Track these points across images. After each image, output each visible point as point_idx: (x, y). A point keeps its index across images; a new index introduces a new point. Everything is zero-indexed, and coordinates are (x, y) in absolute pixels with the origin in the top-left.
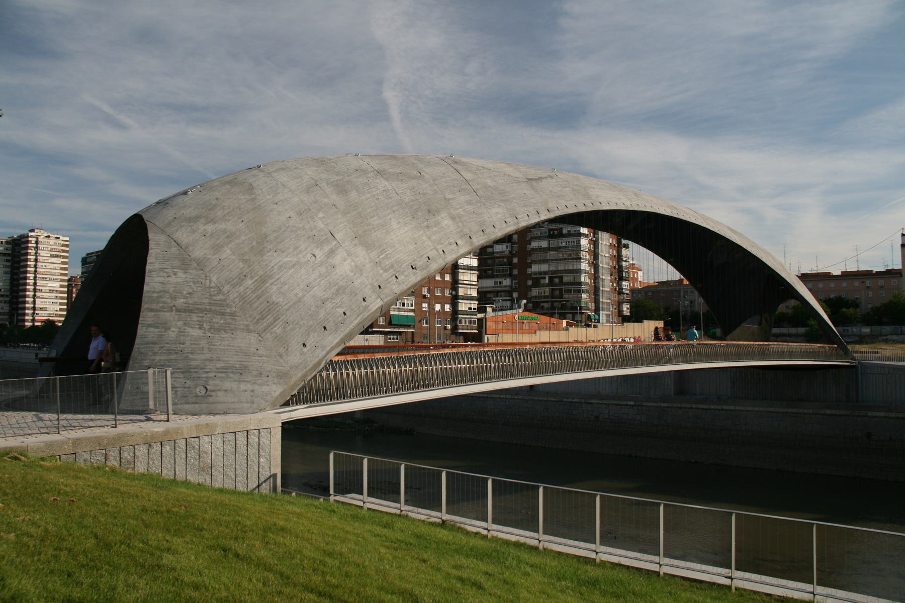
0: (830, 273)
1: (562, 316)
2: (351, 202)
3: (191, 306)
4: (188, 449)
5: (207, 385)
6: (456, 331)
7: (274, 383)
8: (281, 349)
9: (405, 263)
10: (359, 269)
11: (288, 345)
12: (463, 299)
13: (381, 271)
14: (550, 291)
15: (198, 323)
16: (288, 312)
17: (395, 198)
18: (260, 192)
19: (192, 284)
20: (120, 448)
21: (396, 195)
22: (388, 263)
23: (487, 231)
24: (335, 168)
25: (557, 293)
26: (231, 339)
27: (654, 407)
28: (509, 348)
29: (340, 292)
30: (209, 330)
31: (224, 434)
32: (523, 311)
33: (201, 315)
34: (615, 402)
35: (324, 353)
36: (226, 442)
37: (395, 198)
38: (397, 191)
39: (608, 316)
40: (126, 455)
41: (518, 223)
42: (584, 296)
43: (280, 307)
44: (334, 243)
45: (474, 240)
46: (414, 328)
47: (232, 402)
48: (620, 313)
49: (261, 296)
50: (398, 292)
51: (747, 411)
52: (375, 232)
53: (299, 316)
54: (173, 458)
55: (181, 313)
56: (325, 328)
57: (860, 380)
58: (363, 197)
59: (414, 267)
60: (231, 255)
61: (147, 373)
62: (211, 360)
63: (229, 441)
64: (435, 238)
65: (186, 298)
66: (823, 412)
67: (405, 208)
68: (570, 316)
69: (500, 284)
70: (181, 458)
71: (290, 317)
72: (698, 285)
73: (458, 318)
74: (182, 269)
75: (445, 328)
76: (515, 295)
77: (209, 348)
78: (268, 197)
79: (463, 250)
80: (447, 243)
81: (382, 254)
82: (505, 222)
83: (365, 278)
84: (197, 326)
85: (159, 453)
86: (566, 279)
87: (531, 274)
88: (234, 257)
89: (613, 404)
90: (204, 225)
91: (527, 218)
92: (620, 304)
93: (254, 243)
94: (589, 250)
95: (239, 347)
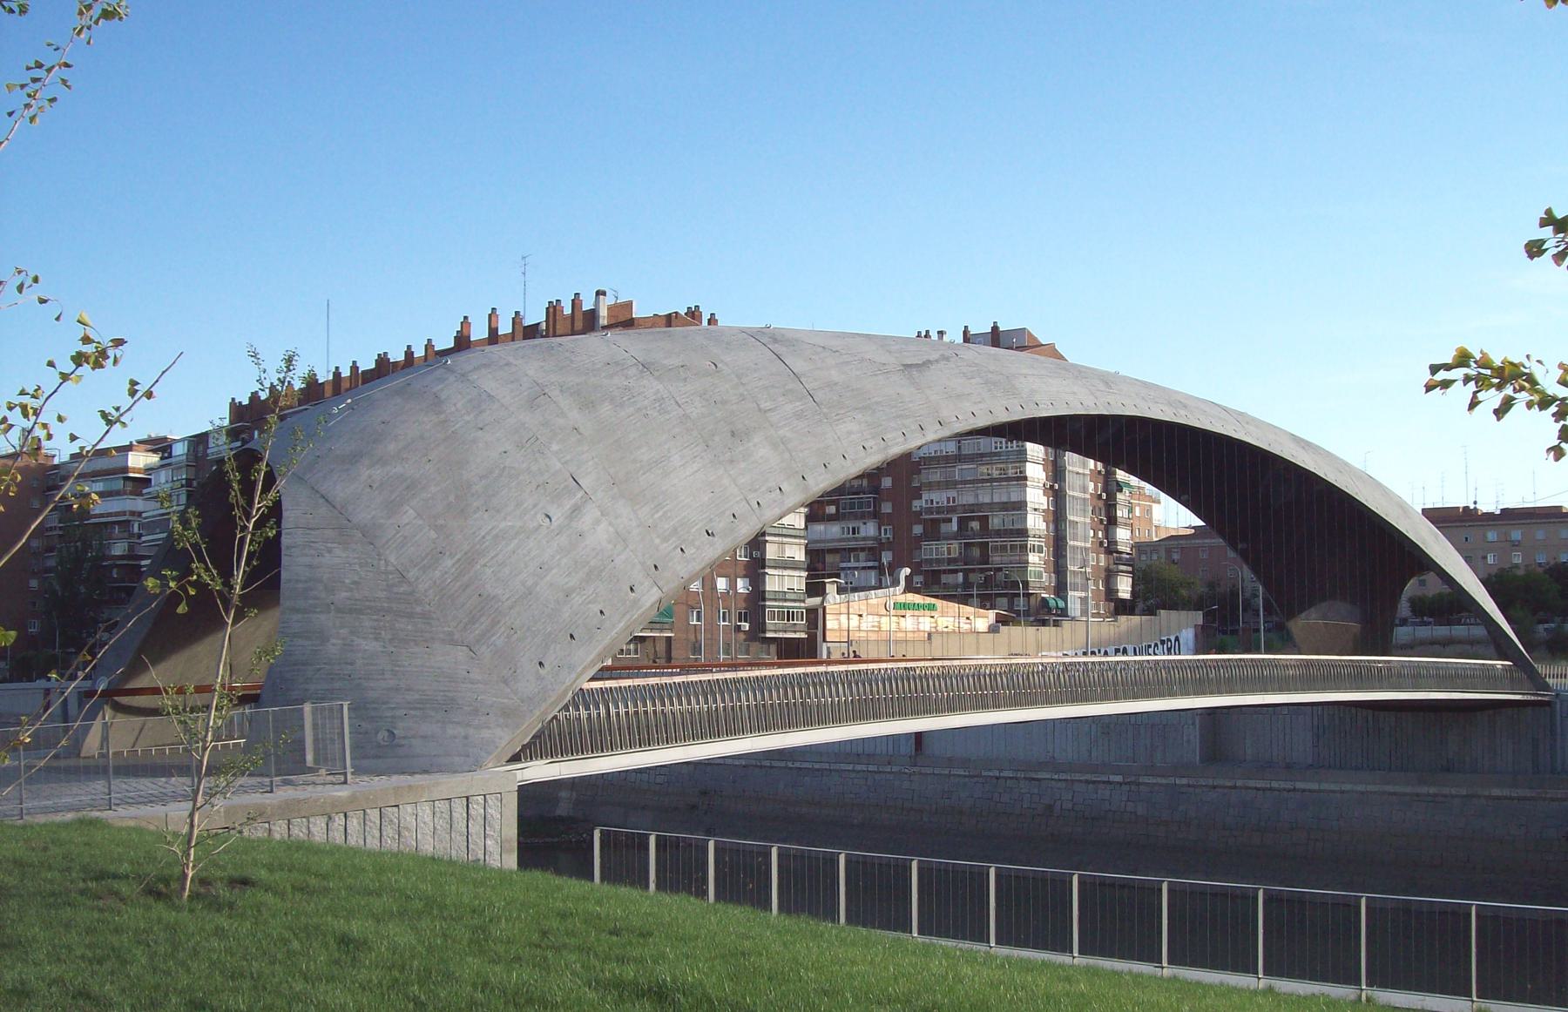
0: (1561, 507)
1: (986, 602)
2: (603, 423)
3: (358, 603)
4: (383, 823)
5: (395, 728)
6: (762, 635)
7: (498, 725)
8: (505, 672)
9: (696, 525)
10: (621, 538)
11: (516, 665)
12: (775, 568)
13: (657, 541)
14: (960, 548)
15: (373, 631)
16: (512, 611)
17: (675, 413)
18: (453, 409)
19: (357, 567)
20: (289, 821)
21: (677, 407)
22: (667, 526)
23: (833, 465)
24: (572, 361)
25: (976, 552)
26: (426, 656)
27: (1161, 785)
28: (1538, 521)
29: (592, 577)
30: (391, 640)
31: (434, 801)
32: (904, 592)
33: (375, 617)
34: (1088, 777)
35: (574, 676)
36: (438, 815)
37: (675, 413)
38: (678, 399)
39: (1084, 600)
40: (296, 832)
41: (885, 449)
42: (1033, 558)
43: (500, 604)
44: (580, 494)
45: (810, 481)
46: (671, 630)
47: (435, 756)
48: (1111, 593)
49: (467, 586)
50: (686, 576)
51: (1342, 792)
52: (644, 474)
53: (531, 618)
54: (362, 836)
55: (345, 615)
56: (572, 636)
57: (1559, 730)
58: (623, 413)
59: (710, 532)
60: (415, 518)
61: (302, 709)
62: (397, 689)
63: (442, 812)
64: (743, 481)
65: (351, 590)
66: (1487, 793)
67: (692, 430)
68: (1004, 601)
69: (854, 533)
70: (373, 837)
71: (516, 620)
72: (1240, 546)
73: (764, 607)
74: (340, 544)
75: (738, 628)
76: (886, 557)
77: (392, 670)
78: (467, 418)
79: (790, 502)
80: (763, 489)
81: (658, 511)
82: (864, 447)
83: (631, 553)
84: (371, 636)
85: (342, 829)
86: (995, 522)
87: (920, 513)
88: (420, 522)
89: (1080, 781)
90: (367, 469)
91: (902, 439)
92: (1110, 576)
93: (452, 498)
94: (1044, 460)
95: (439, 668)
